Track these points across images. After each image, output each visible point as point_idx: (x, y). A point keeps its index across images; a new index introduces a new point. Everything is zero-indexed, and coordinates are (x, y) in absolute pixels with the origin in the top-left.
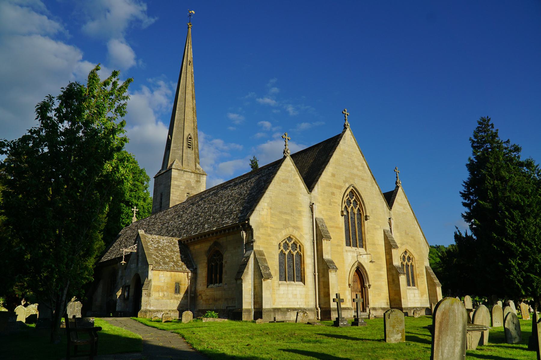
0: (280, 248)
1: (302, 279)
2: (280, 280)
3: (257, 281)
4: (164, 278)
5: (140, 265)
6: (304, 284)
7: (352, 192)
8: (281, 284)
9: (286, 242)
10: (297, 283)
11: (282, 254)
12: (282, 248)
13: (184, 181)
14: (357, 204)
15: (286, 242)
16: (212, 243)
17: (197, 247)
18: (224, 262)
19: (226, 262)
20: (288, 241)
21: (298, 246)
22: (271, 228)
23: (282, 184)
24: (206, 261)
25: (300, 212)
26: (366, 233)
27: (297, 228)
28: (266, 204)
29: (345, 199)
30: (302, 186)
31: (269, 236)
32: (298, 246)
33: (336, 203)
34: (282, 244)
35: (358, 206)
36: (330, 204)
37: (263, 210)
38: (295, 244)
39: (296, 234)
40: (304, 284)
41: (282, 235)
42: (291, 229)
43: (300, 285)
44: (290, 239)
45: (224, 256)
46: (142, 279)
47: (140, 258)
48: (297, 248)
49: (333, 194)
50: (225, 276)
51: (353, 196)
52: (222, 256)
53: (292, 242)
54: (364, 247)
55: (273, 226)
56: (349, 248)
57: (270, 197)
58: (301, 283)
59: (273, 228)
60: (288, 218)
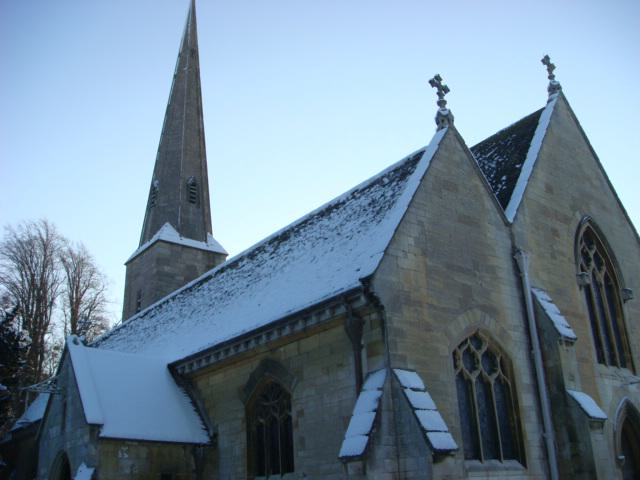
0: (456, 367)
1: (516, 451)
2: (466, 459)
3: (500, 473)
4: (130, 463)
5: (69, 428)
6: (524, 464)
7: (588, 232)
8: (472, 469)
9: (468, 349)
10: (507, 463)
11: (463, 381)
12: (461, 364)
13: (182, 266)
14: (602, 264)
15: (468, 349)
16: (256, 363)
17: (217, 379)
18: (293, 414)
19: (301, 413)
20: (473, 348)
21: (498, 359)
22: (431, 306)
23: (445, 193)
24: (242, 415)
25: (492, 270)
26: (629, 331)
27: (492, 311)
28: (411, 241)
29: (580, 248)
30: (489, 204)
31: (428, 329)
32: (498, 359)
33: (563, 254)
34: (460, 353)
35: (604, 268)
36: (553, 257)
37: (406, 257)
38: (489, 356)
39: (491, 325)
40: (524, 464)
41: (461, 326)
42: (479, 313)
43: (516, 469)
44: (476, 339)
45: (294, 397)
46: (72, 466)
47: (70, 408)
48: (496, 366)
49: (555, 232)
50: (301, 454)
51: (592, 243)
52: (288, 397)
53: (484, 348)
54: (629, 364)
55: (435, 303)
56: (602, 368)
57: (420, 223)
58: (515, 463)
59: (435, 308)
60: (469, 283)
